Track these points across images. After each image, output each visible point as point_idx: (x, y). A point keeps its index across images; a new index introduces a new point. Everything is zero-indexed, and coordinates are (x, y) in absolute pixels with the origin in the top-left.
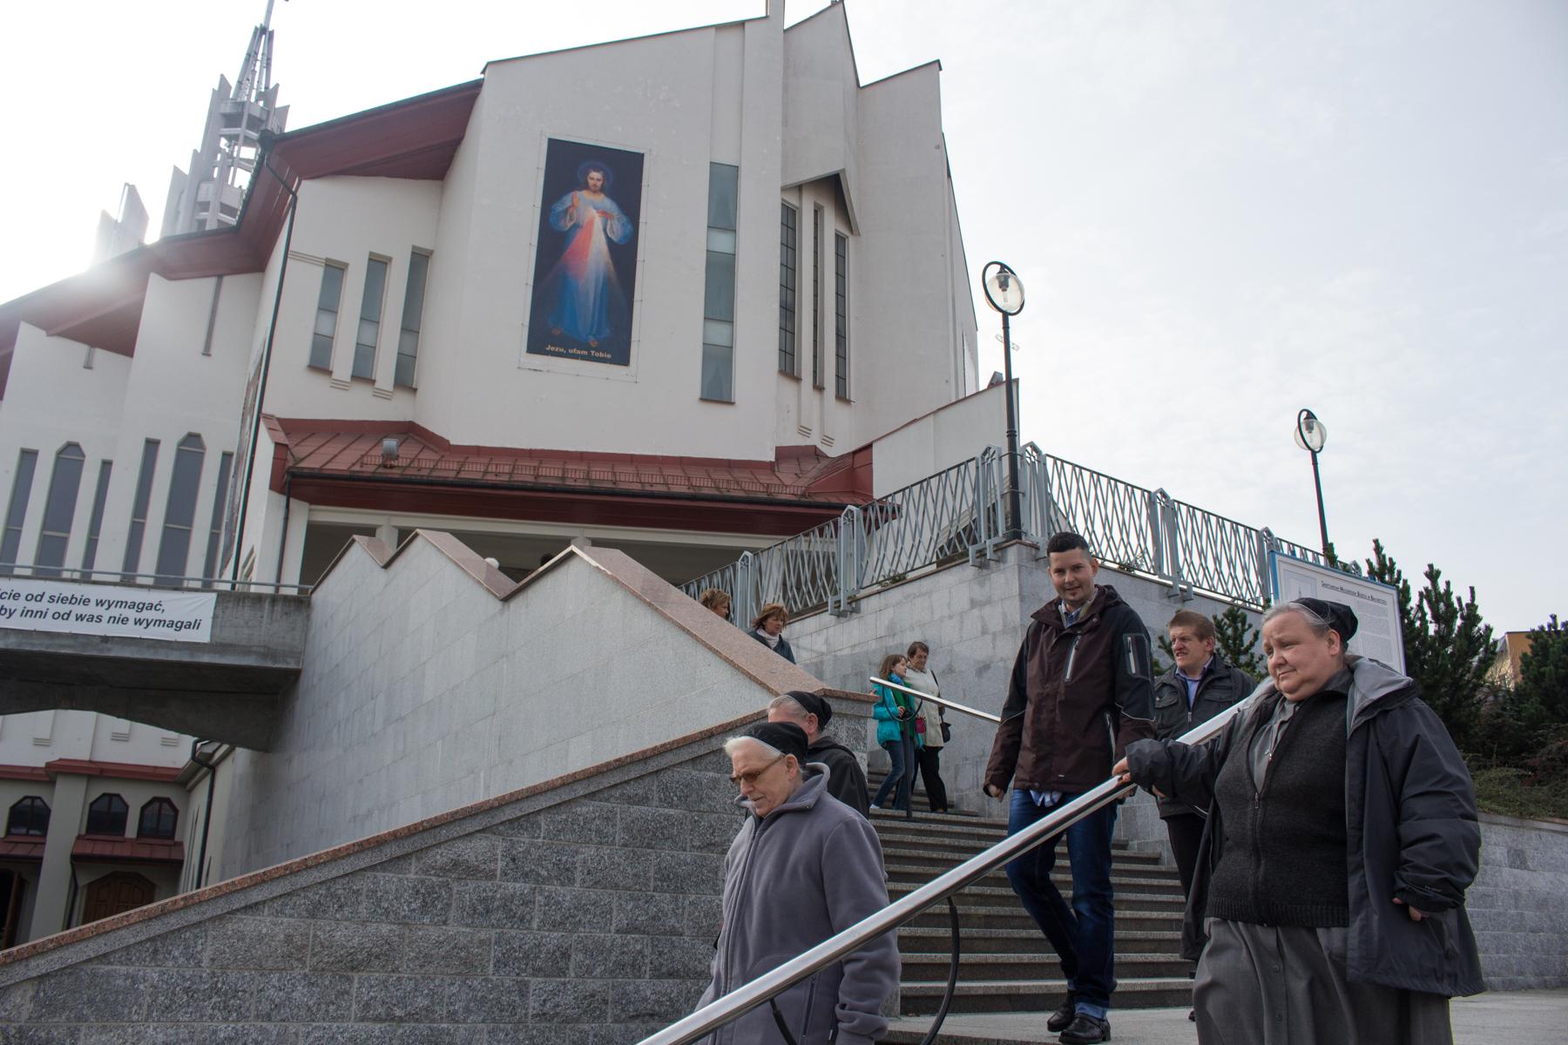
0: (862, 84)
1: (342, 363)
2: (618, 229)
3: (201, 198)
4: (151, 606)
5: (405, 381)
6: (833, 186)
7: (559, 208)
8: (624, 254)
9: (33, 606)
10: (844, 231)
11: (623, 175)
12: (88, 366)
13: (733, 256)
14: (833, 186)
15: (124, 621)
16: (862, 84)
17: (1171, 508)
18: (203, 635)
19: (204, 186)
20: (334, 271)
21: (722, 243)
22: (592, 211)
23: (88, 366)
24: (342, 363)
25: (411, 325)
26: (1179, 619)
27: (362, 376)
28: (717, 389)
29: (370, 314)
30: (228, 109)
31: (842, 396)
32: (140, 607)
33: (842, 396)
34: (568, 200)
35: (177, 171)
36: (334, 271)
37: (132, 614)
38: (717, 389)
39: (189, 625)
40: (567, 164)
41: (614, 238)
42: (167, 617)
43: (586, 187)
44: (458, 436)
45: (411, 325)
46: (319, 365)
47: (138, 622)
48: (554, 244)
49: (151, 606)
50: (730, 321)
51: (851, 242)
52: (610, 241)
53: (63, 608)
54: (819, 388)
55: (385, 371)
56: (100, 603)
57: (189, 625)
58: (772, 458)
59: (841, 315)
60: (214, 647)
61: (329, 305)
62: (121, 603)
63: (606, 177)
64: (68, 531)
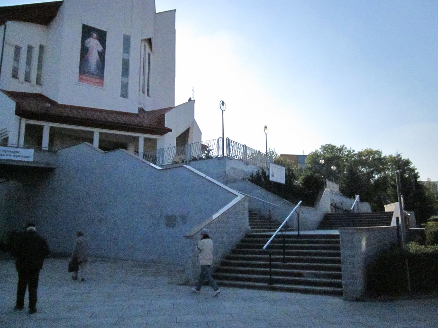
0: (156, 12)
1: (21, 75)
2: (100, 48)
4: (17, 152)
5: (38, 82)
6: (149, 41)
8: (102, 55)
10: (150, 52)
13: (128, 60)
14: (149, 41)
15: (10, 155)
16: (156, 12)
17: (246, 147)
18: (31, 159)
20: (18, 50)
21: (126, 56)
22: (93, 44)
24: (21, 75)
25: (40, 67)
27: (27, 79)
28: (124, 95)
29: (29, 63)
31: (148, 95)
32: (15, 152)
33: (148, 95)
36: (18, 50)
37: (12, 154)
38: (124, 95)
39: (27, 157)
41: (100, 50)
42: (21, 155)
43: (93, 37)
44: (61, 101)
45: (40, 67)
47: (14, 156)
48: (84, 51)
49: (17, 152)
50: (128, 77)
51: (152, 55)
52: (98, 51)
54: (144, 93)
55: (33, 77)
56: (3, 151)
57: (27, 157)
58: (137, 112)
60: (33, 162)
63: (97, 35)
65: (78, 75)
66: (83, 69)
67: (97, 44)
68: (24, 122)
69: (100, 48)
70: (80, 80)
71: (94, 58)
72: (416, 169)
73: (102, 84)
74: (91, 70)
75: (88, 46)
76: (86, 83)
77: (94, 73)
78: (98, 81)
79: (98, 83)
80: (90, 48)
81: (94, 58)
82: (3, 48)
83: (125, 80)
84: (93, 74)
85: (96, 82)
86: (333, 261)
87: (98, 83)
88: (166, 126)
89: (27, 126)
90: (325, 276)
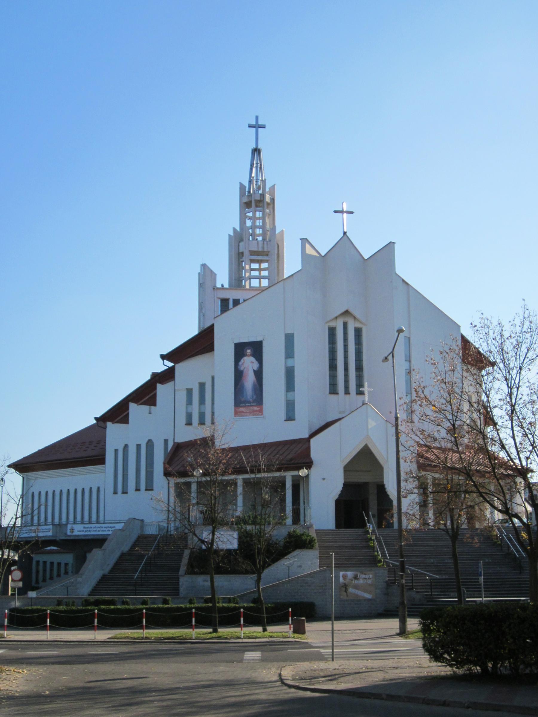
1: (195, 419)
2: (256, 366)
3: (241, 251)
7: (240, 363)
8: (259, 374)
9: (94, 529)
11: (256, 348)
12: (150, 413)
18: (50, 534)
19: (241, 244)
20: (189, 392)
22: (249, 363)
23: (150, 413)
24: (195, 419)
26: (473, 428)
28: (290, 417)
30: (245, 200)
34: (242, 361)
35: (230, 235)
36: (189, 392)
38: (290, 417)
40: (240, 350)
43: (246, 355)
46: (189, 423)
48: (239, 375)
52: (254, 370)
53: (99, 529)
59: (359, 353)
61: (189, 402)
62: (108, 527)
64: (153, 468)
65: (233, 407)
66: (239, 401)
67: (252, 362)
68: (173, 481)
69: (256, 366)
70: (236, 413)
71: (250, 380)
73: (261, 412)
74: (248, 398)
75: (242, 369)
76: (242, 416)
77: (251, 400)
78: (256, 408)
79: (256, 411)
80: (245, 371)
81: (250, 380)
83: (290, 363)
84: (249, 402)
85: (254, 411)
86: (488, 585)
87: (256, 411)
89: (177, 484)
90: (440, 585)
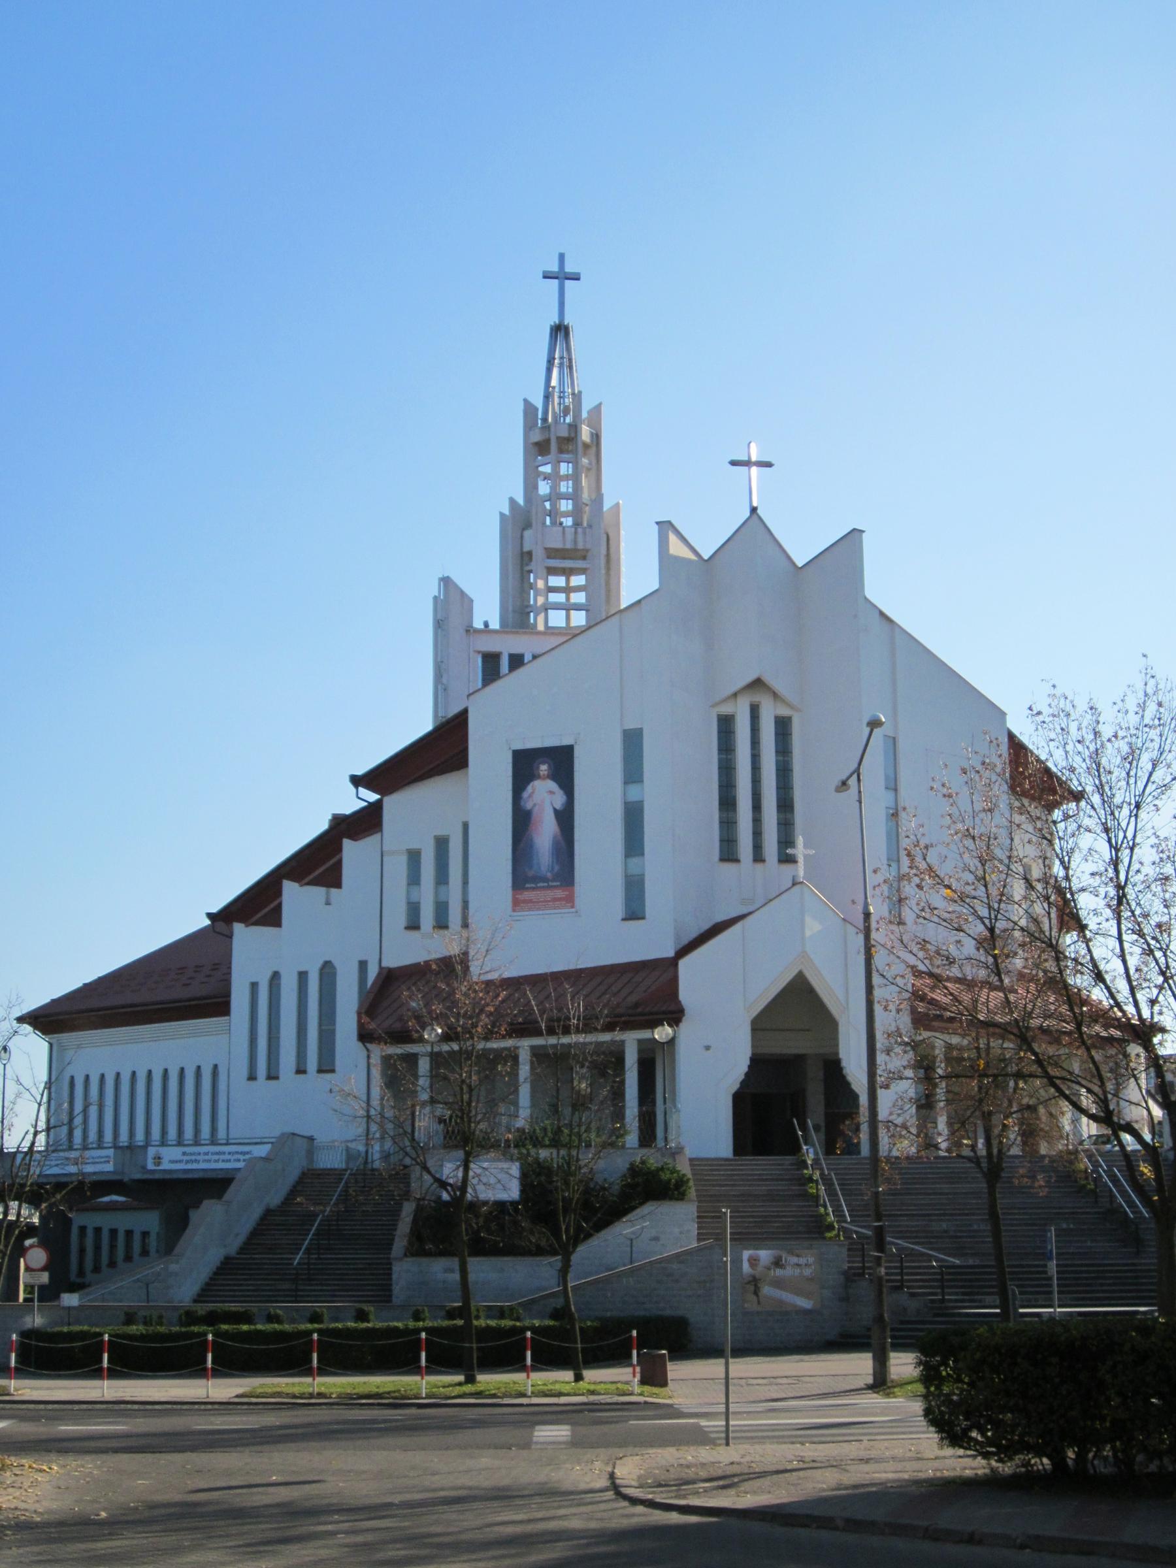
1: (427, 917)
2: (559, 800)
3: (526, 549)
7: (525, 795)
8: (565, 818)
9: (206, 1157)
11: (560, 762)
12: (328, 903)
19: (527, 533)
20: (414, 857)
22: (544, 794)
23: (328, 903)
24: (427, 917)
28: (634, 912)
30: (537, 437)
34: (529, 789)
35: (502, 514)
36: (414, 857)
38: (634, 912)
40: (525, 765)
43: (539, 777)
46: (413, 925)
48: (522, 821)
52: (555, 810)
53: (216, 1157)
59: (784, 772)
61: (414, 878)
62: (237, 1153)
64: (334, 1024)
65: (510, 891)
66: (523, 876)
67: (551, 792)
68: (378, 1051)
69: (559, 800)
70: (516, 904)
71: (545, 831)
72: (512, 502)
73: (570, 900)
74: (543, 870)
75: (529, 806)
76: (530, 910)
77: (549, 875)
78: (559, 893)
79: (560, 899)
80: (535, 810)
81: (545, 831)
82: (553, 649)
83: (634, 793)
84: (545, 879)
85: (555, 900)
87: (560, 899)
88: (656, 586)
89: (386, 1059)
